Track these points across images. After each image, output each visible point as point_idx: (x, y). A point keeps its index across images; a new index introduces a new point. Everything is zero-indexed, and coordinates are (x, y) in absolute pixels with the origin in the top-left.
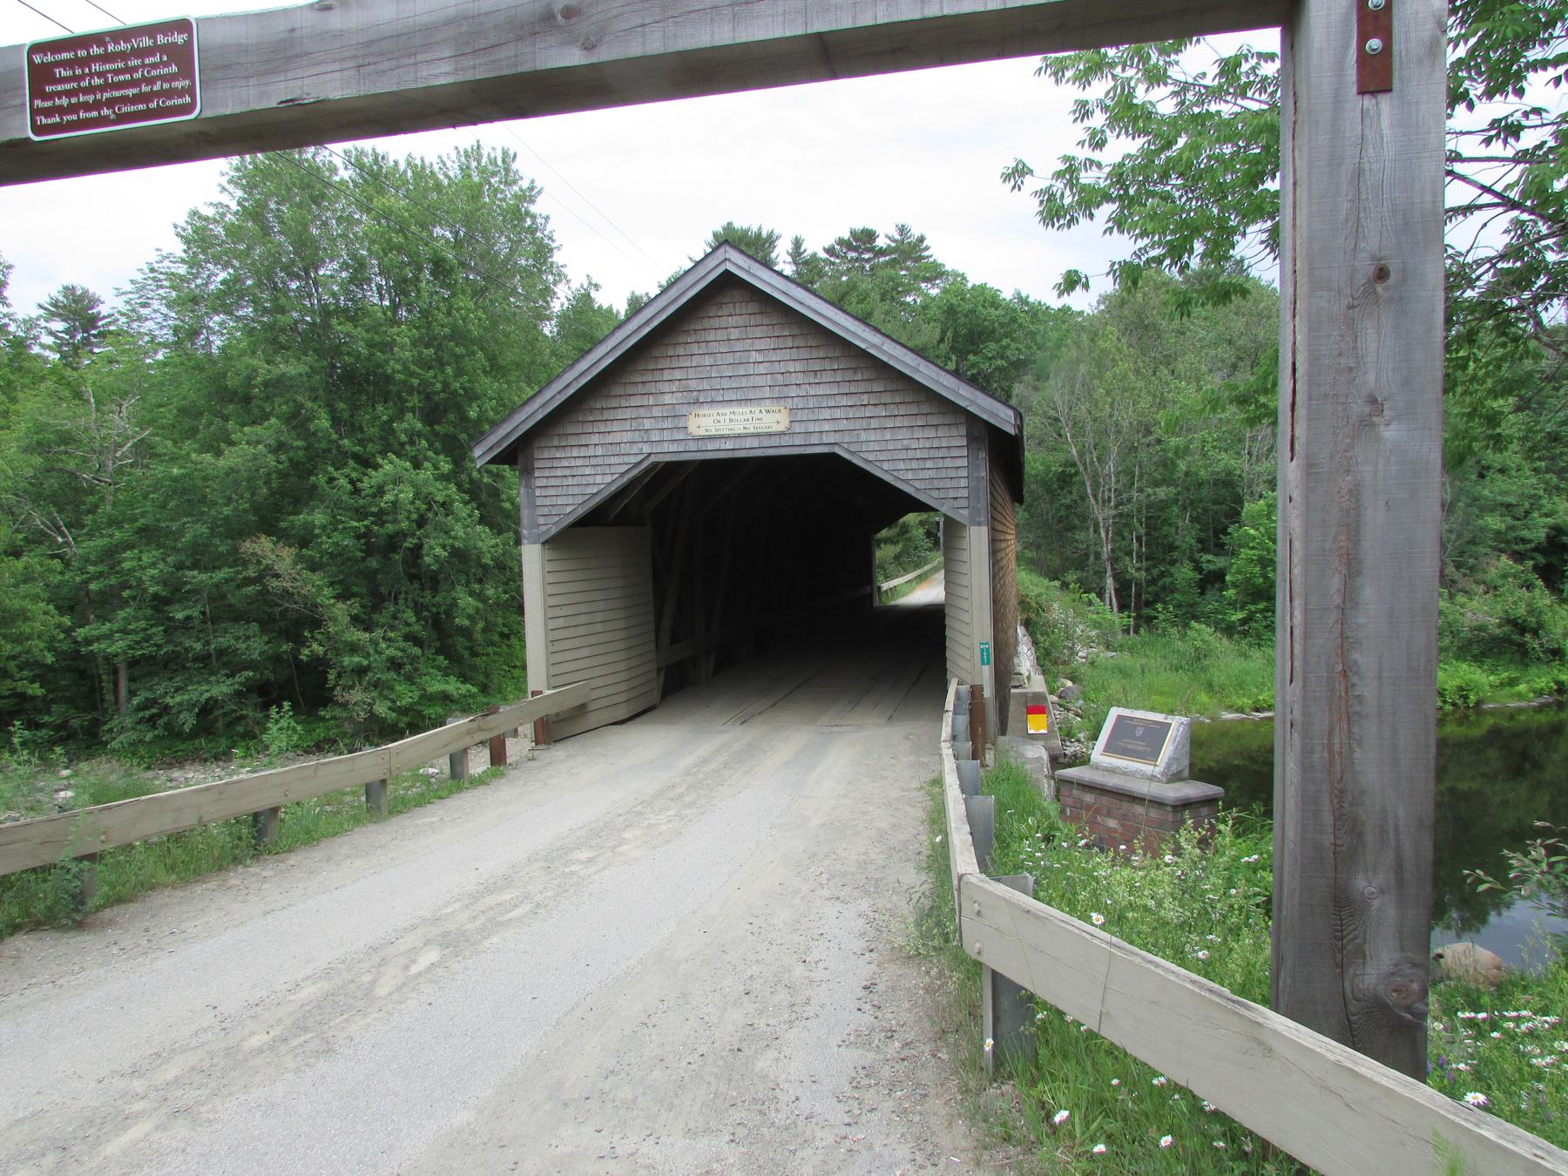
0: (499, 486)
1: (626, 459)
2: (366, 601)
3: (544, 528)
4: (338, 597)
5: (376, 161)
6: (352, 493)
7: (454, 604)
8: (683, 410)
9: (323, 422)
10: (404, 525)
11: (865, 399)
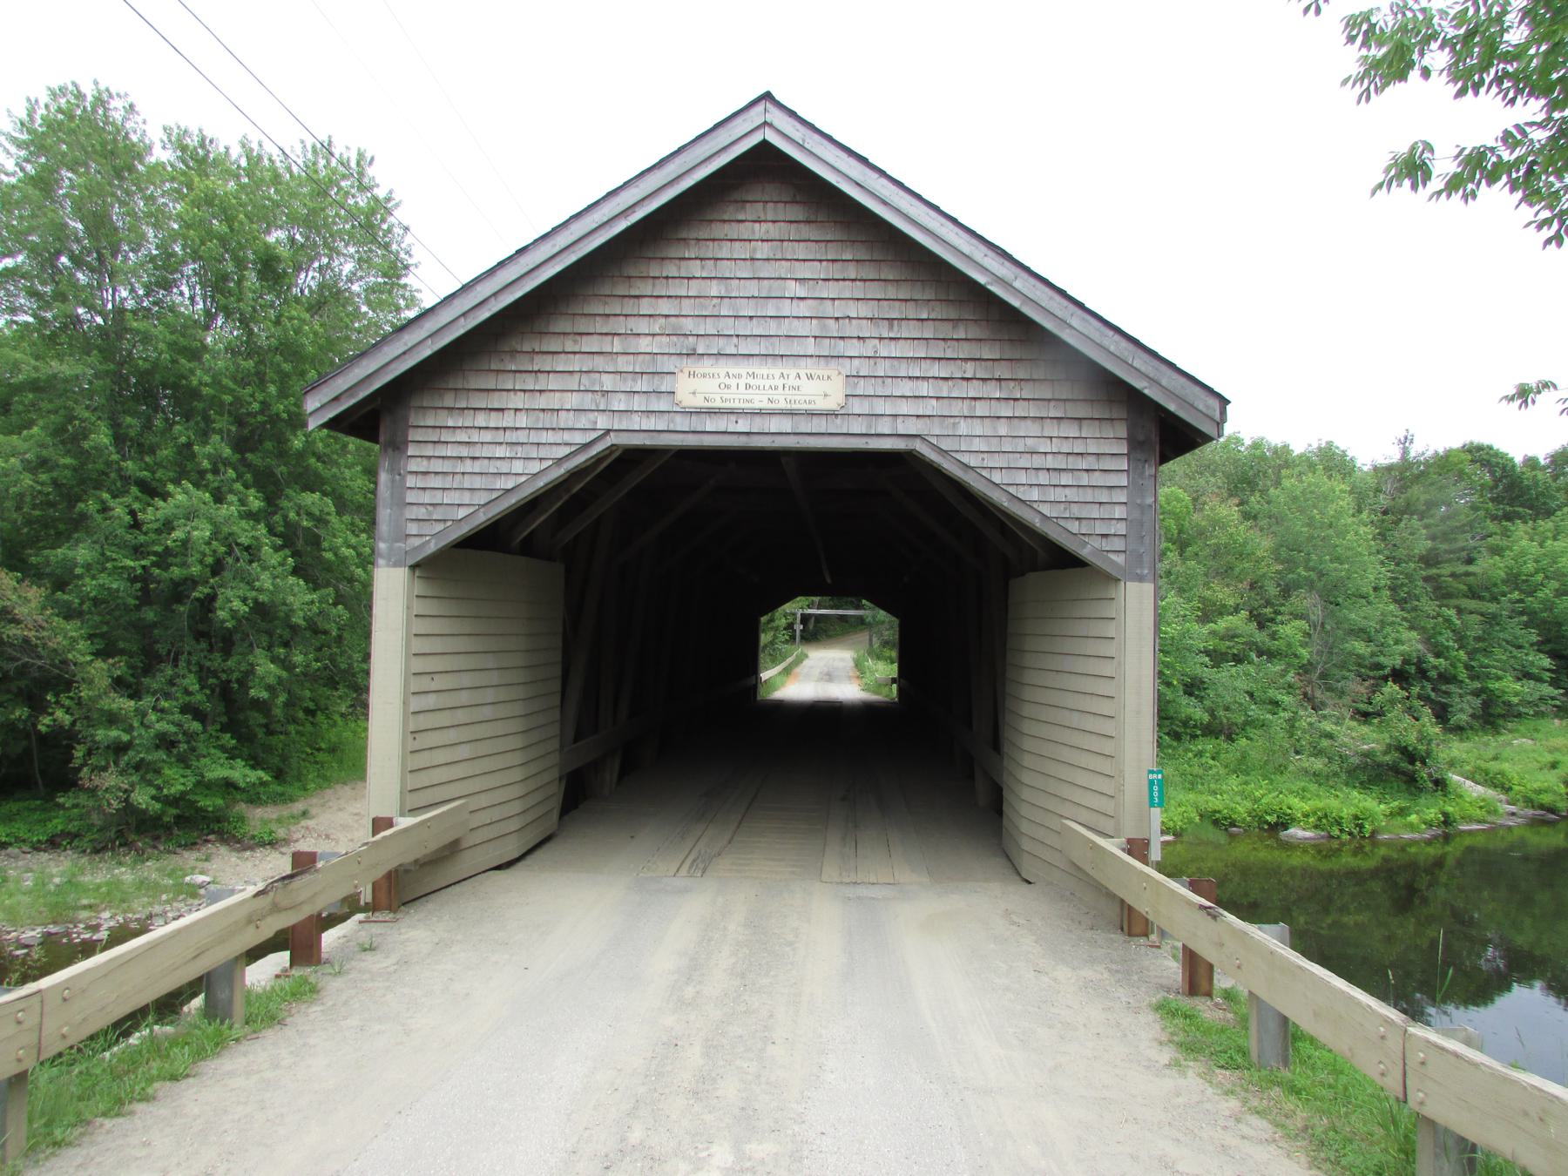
0: (322, 532)
1: (567, 437)
2: (137, 661)
3: (417, 542)
4: (97, 654)
5: (202, 145)
6: (131, 527)
7: (251, 671)
8: (668, 364)
9: (102, 437)
10: (195, 570)
11: (970, 370)
